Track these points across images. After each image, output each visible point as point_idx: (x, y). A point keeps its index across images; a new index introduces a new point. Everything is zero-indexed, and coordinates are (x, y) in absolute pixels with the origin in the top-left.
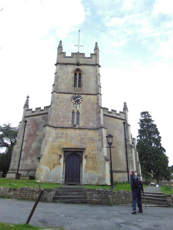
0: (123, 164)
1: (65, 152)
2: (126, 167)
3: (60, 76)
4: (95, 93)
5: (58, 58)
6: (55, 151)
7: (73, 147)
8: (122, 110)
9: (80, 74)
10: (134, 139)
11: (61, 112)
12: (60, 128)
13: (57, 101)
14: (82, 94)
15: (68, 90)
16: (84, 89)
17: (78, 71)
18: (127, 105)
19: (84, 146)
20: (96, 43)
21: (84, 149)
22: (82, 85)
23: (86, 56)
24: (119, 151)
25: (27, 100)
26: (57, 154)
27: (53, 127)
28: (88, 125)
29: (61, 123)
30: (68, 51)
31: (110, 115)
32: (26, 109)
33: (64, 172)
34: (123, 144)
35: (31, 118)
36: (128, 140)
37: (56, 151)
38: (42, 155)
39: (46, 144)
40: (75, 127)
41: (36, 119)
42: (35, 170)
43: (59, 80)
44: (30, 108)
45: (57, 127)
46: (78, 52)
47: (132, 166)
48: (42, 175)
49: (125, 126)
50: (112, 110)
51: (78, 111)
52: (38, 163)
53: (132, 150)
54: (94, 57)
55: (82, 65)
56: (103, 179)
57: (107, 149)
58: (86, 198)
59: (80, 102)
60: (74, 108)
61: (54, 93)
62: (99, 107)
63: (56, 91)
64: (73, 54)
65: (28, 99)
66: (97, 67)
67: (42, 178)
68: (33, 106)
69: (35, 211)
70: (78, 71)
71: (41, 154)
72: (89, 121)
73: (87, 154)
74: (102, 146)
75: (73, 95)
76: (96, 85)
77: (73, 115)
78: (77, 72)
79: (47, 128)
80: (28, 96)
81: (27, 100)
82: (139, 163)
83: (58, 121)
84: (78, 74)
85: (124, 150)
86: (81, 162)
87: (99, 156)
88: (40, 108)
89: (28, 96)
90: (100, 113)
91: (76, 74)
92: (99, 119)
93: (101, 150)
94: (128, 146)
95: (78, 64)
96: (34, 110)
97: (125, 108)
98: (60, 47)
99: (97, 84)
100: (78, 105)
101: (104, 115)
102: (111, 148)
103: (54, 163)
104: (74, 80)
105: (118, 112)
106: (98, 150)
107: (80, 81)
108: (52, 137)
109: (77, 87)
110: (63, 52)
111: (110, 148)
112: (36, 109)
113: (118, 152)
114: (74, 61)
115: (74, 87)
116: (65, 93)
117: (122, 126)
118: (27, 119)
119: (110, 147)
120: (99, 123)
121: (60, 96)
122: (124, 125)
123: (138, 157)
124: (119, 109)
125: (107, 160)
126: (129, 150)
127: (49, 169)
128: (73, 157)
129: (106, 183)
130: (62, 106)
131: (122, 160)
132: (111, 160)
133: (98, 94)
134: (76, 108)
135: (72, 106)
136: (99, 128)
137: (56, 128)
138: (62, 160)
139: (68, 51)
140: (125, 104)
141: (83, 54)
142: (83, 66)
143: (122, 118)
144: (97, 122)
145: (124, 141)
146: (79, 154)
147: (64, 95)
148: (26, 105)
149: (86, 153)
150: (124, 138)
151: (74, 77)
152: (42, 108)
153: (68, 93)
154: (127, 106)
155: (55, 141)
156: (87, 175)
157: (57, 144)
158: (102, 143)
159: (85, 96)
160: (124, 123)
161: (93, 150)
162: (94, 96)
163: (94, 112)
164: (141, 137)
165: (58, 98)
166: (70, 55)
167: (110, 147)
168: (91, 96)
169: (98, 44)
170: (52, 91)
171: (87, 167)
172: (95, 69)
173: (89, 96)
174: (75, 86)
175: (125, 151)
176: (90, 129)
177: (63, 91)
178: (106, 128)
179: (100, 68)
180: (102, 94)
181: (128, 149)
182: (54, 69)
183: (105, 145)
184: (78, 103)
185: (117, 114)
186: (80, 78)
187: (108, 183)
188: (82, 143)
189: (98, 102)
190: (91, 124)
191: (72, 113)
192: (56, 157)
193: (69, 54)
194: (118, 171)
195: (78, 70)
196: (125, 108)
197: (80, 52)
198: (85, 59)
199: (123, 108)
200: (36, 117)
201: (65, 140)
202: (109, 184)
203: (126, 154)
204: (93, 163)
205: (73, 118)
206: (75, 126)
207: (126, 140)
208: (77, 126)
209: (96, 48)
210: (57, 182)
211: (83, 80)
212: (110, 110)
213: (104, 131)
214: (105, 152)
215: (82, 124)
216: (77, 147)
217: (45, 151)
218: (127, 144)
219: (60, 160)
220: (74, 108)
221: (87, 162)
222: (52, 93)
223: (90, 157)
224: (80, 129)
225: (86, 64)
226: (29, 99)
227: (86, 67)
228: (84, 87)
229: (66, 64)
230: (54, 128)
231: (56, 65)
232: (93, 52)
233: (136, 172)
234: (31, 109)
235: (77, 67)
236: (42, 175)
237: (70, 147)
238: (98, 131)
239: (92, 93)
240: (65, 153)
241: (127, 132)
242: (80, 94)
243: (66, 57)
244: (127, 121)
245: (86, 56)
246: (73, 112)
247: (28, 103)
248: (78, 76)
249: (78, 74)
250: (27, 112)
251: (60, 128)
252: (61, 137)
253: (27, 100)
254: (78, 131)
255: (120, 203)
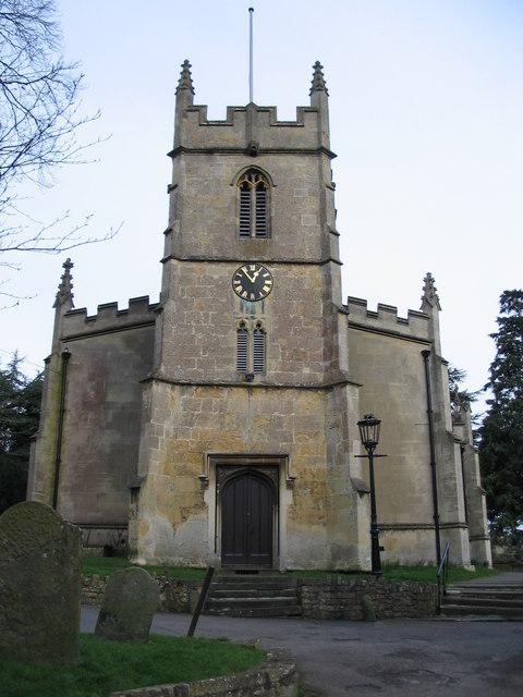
0: (420, 500)
1: (218, 466)
2: (431, 512)
3: (188, 197)
4: (318, 258)
5: (178, 129)
6: (185, 466)
7: (247, 450)
8: (417, 306)
9: (260, 187)
10: (463, 400)
11: (199, 329)
12: (198, 385)
13: (183, 290)
14: (270, 263)
15: (220, 250)
16: (280, 244)
17: (253, 176)
18: (435, 285)
19: (282, 447)
20: (318, 66)
21: (285, 456)
22: (271, 229)
23: (282, 117)
24: (406, 455)
25: (67, 277)
26: (192, 474)
27: (175, 384)
28: (295, 374)
29: (201, 370)
30: (216, 101)
31: (374, 323)
32: (64, 311)
33: (219, 534)
34: (423, 429)
35: (83, 342)
36: (439, 416)
37: (189, 465)
38: (144, 480)
39: (155, 443)
40: (249, 380)
41: (113, 348)
42: (125, 526)
43: (188, 212)
44: (78, 305)
45: (190, 385)
46: (251, 104)
47: (452, 506)
48: (148, 543)
49: (430, 365)
50: (381, 307)
51: (259, 325)
52: (132, 506)
53: (452, 450)
54: (310, 119)
55: (267, 151)
56: (350, 552)
57: (362, 462)
58: (300, 603)
59: (264, 292)
60: (244, 315)
61: (174, 262)
62: (335, 311)
63: (176, 254)
64: (232, 111)
65: (67, 271)
66: (324, 157)
67: (151, 550)
68: (88, 299)
69: (370, 551)
70: (253, 176)
71: (140, 475)
72: (299, 360)
73: (293, 473)
74: (347, 448)
75: (238, 266)
76: (319, 226)
77: (242, 340)
78: (250, 180)
79: (157, 388)
80: (69, 259)
81: (67, 277)
82: (483, 493)
83: (189, 363)
84: (253, 184)
85: (426, 453)
86: (275, 499)
87: (336, 479)
88: (115, 305)
89: (69, 259)
90: (335, 329)
91: (245, 188)
92: (331, 351)
93: (341, 460)
94: (437, 438)
95: (252, 151)
96: (92, 312)
97: (430, 298)
98: (185, 87)
99: (322, 226)
100: (258, 305)
101: (352, 325)
102: (375, 459)
103: (183, 506)
104: (239, 208)
105: (403, 314)
106: (329, 460)
107: (262, 211)
108: (172, 417)
109: (253, 235)
110: (195, 103)
111: (371, 460)
112: (101, 308)
113: (402, 461)
114: (236, 137)
115: (242, 239)
116: (210, 261)
117: (416, 366)
118: (70, 347)
119: (371, 456)
120: (335, 365)
121: (192, 270)
122: (426, 361)
123: (478, 473)
124: (408, 301)
125: (362, 493)
126: (441, 454)
127: (169, 525)
128: (249, 483)
129: (358, 566)
130: (202, 309)
131: (417, 488)
132: (372, 492)
133: (327, 260)
134: (253, 312)
135: (237, 310)
136: (333, 385)
137: (185, 388)
138: (210, 496)
139: (216, 101)
140: (429, 280)
141: (270, 111)
142: (271, 157)
143: (417, 331)
144: (328, 363)
145: (426, 421)
146: (267, 472)
147: (208, 267)
148: (65, 295)
149: (292, 470)
150: (423, 407)
151: (239, 197)
152: (123, 306)
153: (219, 261)
154: (435, 290)
155: (184, 433)
156: (298, 538)
157: (190, 440)
158: (346, 436)
159: (283, 268)
160: (425, 354)
161: (315, 461)
162: (314, 268)
163: (316, 328)
164: (497, 391)
165: (185, 280)
166: (223, 117)
167: (371, 456)
168: (303, 268)
169: (322, 70)
170: (165, 254)
171: (293, 517)
172: (314, 169)
173: (295, 268)
174: (245, 231)
175: (429, 454)
176: (302, 388)
177: (201, 252)
178: (359, 385)
179: (333, 161)
180: (341, 260)
181: (438, 448)
182: (165, 171)
183: (357, 447)
184: (257, 296)
185: (401, 321)
186: (262, 201)
187: (366, 563)
188: (275, 438)
189: (327, 290)
190: (306, 371)
191: (239, 331)
192: (191, 485)
193: (217, 113)
194: (403, 525)
195: (254, 172)
196: (430, 298)
197: (260, 102)
198: (279, 129)
199: (423, 298)
200: (100, 339)
201: (219, 425)
202: (369, 567)
203: (433, 464)
204: (316, 501)
205: (242, 350)
206: (250, 377)
207: (432, 416)
208: (257, 380)
209: (318, 86)
210: (197, 566)
211: (275, 209)
212: (372, 307)
213: (351, 395)
214: (356, 468)
215: (273, 370)
216: (259, 450)
217: (157, 464)
218: (436, 430)
219: (202, 494)
220: (245, 315)
221: (295, 500)
222: (163, 261)
223: (306, 484)
224: (267, 387)
225: (283, 150)
226: (72, 271)
227: (283, 162)
228: (276, 237)
229: (210, 152)
230: (177, 387)
231: (172, 155)
232: (307, 102)
233: (464, 528)
234: (84, 311)
235: (248, 161)
236: (148, 543)
237: (237, 451)
238: (329, 395)
239: (308, 258)
240: (219, 469)
241: (436, 386)
242: (264, 262)
243: (209, 124)
244: (436, 346)
245: (282, 117)
246: (242, 328)
247: (71, 286)
248: (254, 193)
249: (255, 184)
250: (67, 321)
251: (198, 385)
252: (204, 419)
253: (64, 277)
254: (260, 397)
255: (396, 615)
